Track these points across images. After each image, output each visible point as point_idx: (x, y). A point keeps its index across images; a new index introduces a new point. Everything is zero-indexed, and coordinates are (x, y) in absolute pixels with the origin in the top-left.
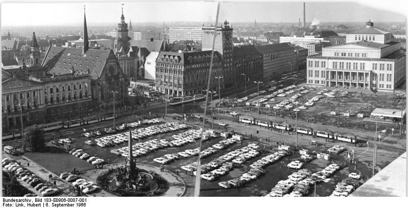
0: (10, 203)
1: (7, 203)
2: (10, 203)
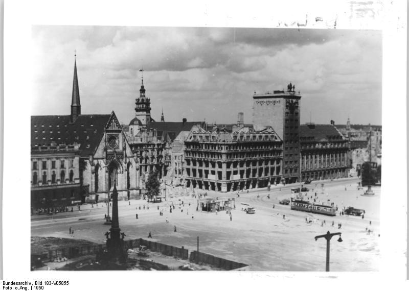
0: (10, 286)
1: (7, 286)
2: (10, 286)
